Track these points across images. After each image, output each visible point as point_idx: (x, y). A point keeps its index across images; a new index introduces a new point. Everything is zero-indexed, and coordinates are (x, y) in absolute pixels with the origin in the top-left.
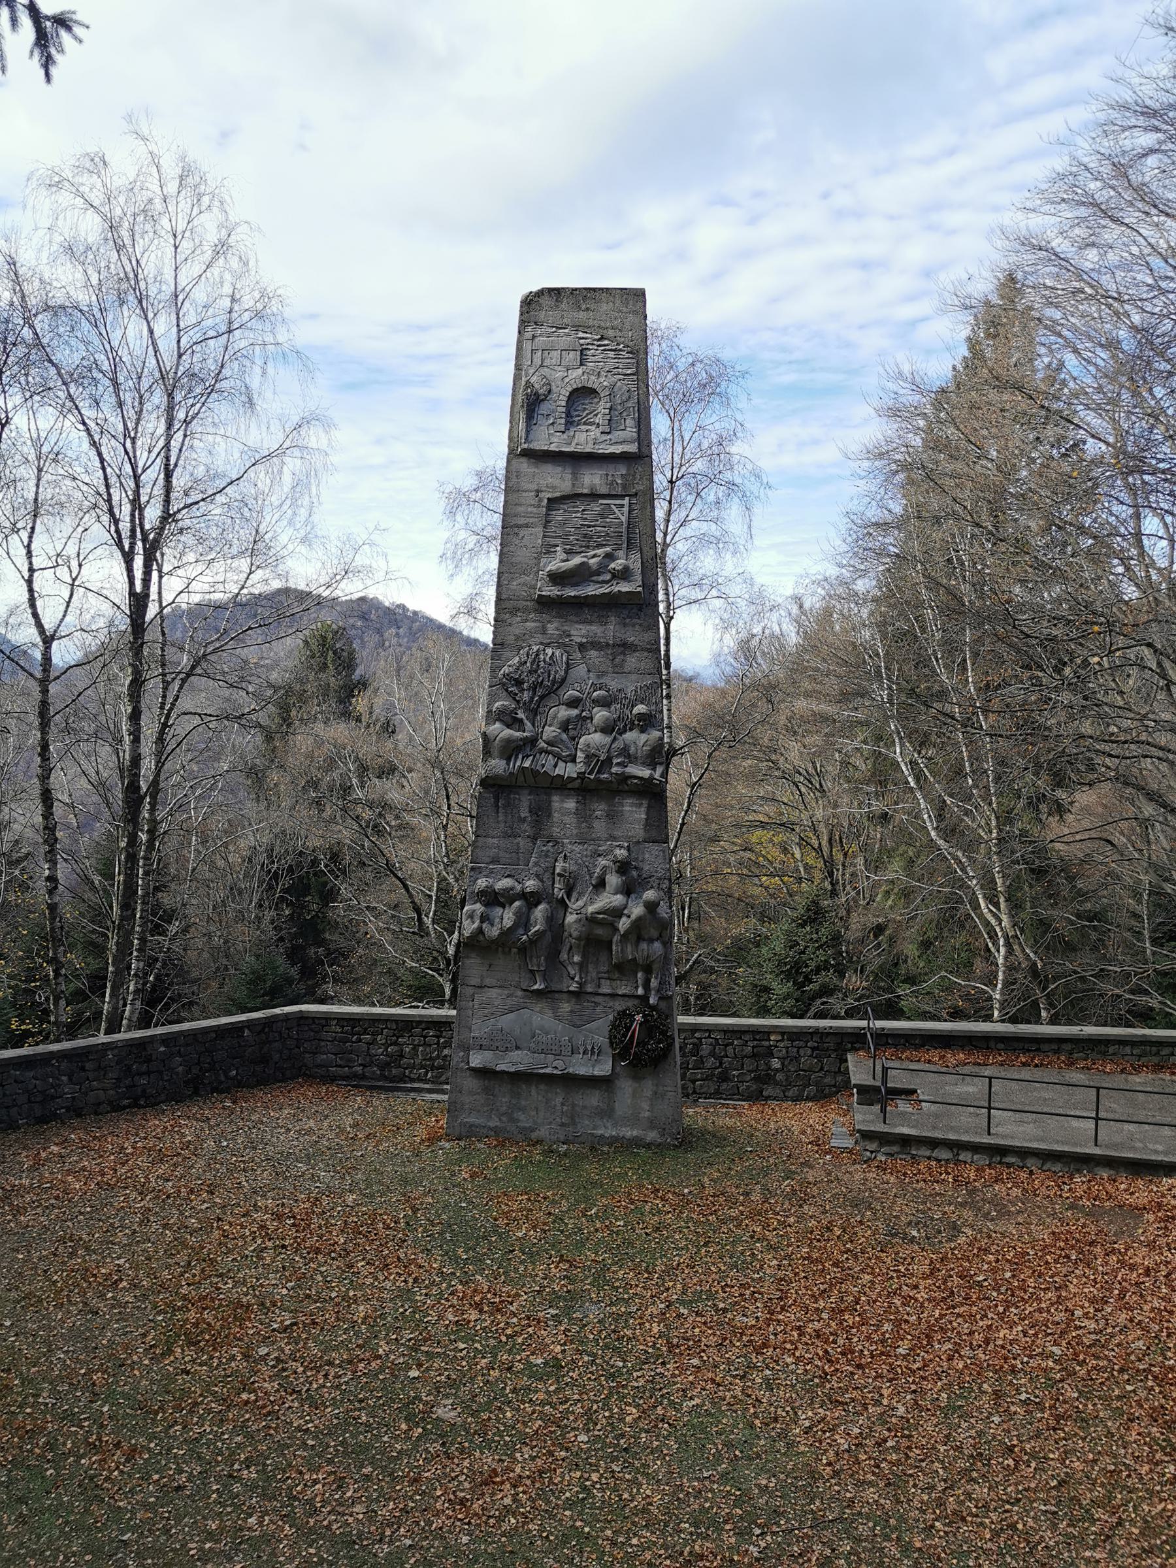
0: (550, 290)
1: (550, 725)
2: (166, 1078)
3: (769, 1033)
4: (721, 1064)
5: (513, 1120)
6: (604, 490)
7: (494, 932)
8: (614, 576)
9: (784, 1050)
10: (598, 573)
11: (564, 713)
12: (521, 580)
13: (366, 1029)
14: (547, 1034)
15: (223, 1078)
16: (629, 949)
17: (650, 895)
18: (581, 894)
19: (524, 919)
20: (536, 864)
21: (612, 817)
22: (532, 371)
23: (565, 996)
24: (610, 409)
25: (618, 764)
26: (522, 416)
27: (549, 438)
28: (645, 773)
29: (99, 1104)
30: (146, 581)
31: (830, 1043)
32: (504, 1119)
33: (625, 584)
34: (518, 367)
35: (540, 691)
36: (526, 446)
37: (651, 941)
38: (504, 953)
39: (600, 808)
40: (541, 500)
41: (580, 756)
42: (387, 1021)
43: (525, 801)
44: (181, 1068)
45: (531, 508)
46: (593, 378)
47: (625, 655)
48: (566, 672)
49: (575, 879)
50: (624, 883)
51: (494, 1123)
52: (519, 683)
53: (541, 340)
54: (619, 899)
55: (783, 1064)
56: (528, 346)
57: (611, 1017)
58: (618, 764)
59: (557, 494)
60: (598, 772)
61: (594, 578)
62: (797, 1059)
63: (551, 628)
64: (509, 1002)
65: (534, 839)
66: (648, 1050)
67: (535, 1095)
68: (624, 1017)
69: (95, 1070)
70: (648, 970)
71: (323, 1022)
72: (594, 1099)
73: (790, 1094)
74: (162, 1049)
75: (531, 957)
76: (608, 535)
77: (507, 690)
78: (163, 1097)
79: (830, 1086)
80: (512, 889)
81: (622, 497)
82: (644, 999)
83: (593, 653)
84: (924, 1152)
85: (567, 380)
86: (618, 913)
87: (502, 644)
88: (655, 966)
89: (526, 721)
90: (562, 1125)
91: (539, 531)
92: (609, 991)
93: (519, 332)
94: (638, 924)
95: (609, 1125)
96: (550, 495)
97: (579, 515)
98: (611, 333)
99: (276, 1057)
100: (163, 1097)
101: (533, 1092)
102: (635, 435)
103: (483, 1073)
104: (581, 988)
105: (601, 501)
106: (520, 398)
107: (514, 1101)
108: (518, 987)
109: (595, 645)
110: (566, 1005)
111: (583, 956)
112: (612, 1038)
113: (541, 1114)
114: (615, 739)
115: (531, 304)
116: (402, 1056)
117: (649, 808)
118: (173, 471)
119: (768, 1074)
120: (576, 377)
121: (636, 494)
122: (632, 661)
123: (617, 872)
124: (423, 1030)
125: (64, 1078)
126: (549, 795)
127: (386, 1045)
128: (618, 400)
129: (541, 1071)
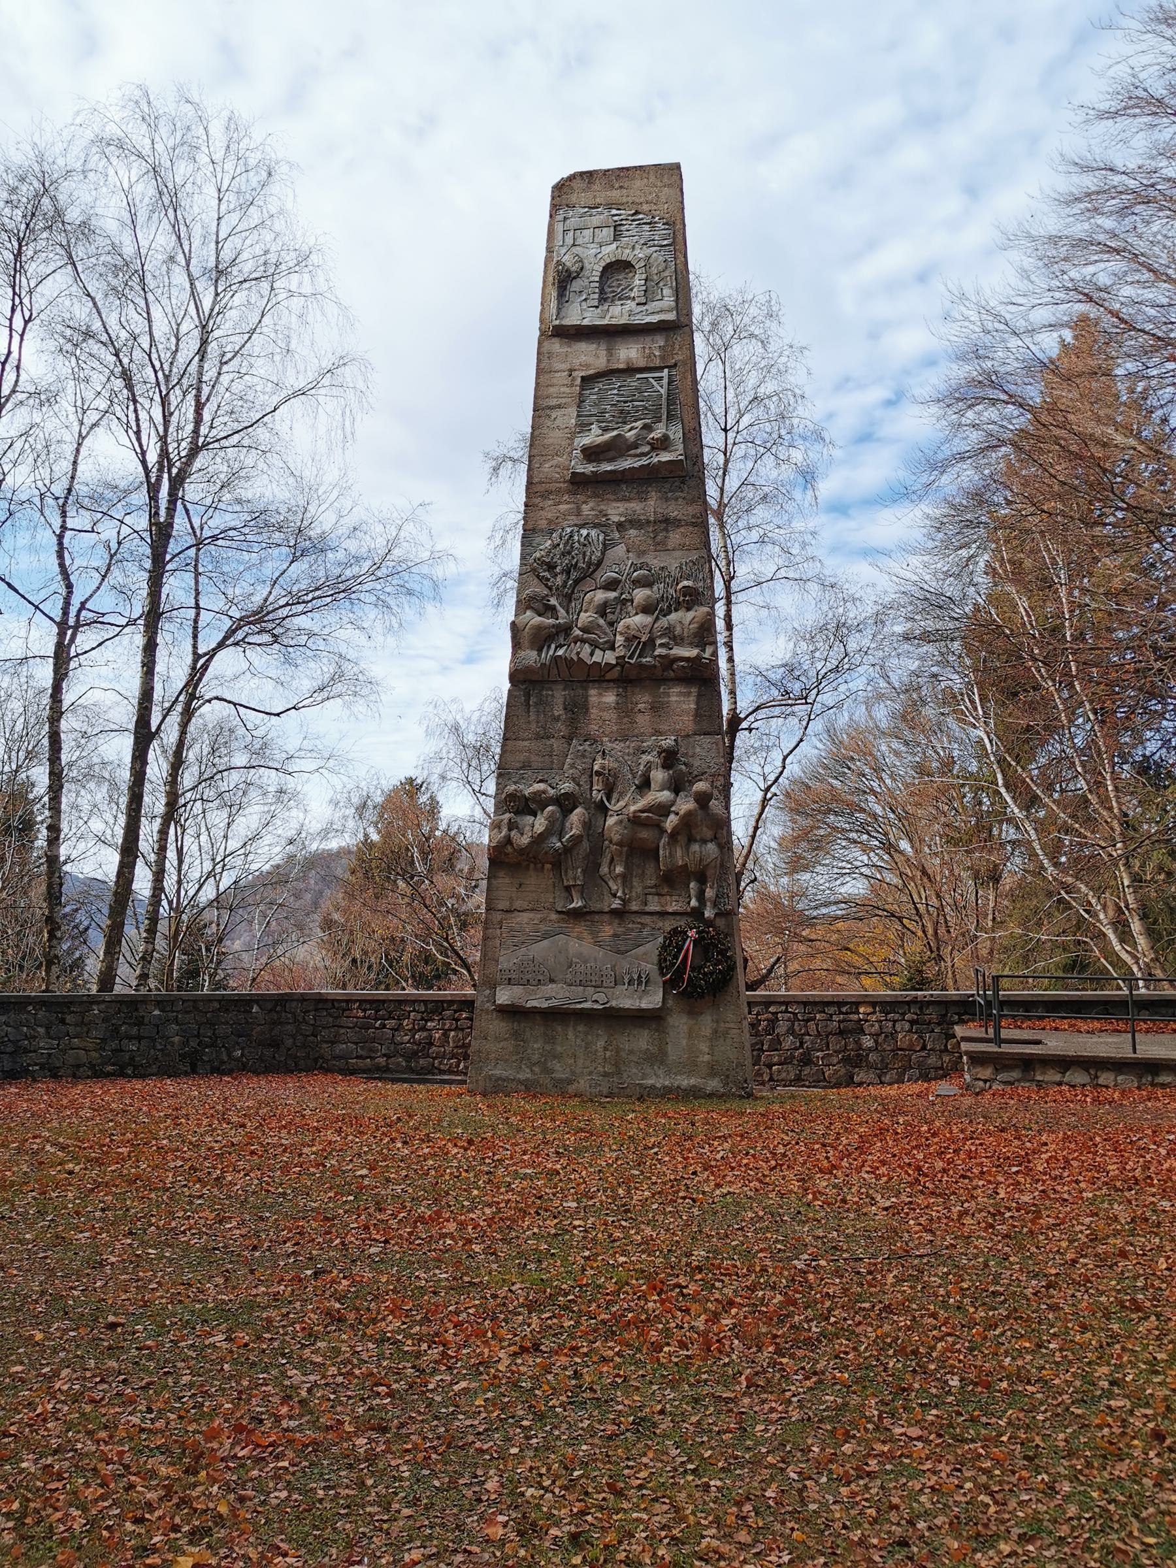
0: (582, 174)
1: (586, 611)
2: (159, 1047)
3: (857, 1004)
4: (802, 1043)
5: (547, 1071)
6: (642, 363)
7: (525, 840)
8: (654, 448)
9: (877, 1025)
10: (635, 446)
11: (601, 596)
12: (554, 462)
13: (391, 1013)
14: (585, 962)
15: (225, 1058)
16: (679, 853)
17: (700, 786)
18: (622, 795)
19: (557, 826)
20: (572, 766)
21: (657, 709)
22: (563, 251)
23: (606, 918)
24: (646, 280)
25: (662, 645)
26: (554, 294)
27: (580, 314)
28: (692, 653)
29: (78, 1066)
30: (171, 510)
31: (932, 1014)
32: (536, 1069)
33: (667, 454)
34: (549, 250)
35: (574, 575)
36: (557, 322)
37: (704, 841)
38: (535, 869)
39: (643, 700)
40: (574, 379)
41: (620, 639)
42: (414, 1001)
43: (559, 696)
44: (177, 1039)
45: (563, 388)
46: (627, 251)
47: (667, 531)
48: (603, 553)
49: (616, 777)
50: (671, 777)
51: (525, 1074)
52: (551, 567)
53: (573, 222)
54: (666, 795)
55: (876, 1042)
56: (559, 227)
57: (661, 940)
58: (662, 645)
59: (591, 372)
60: (640, 656)
61: (632, 452)
62: (893, 1035)
63: (586, 509)
64: (543, 927)
65: (569, 739)
66: (705, 974)
67: (571, 1037)
68: (675, 938)
69: (76, 1025)
70: (702, 879)
71: (344, 1005)
72: (642, 1040)
73: (887, 1078)
74: (157, 1012)
75: (566, 872)
76: (646, 408)
77: (538, 576)
78: (154, 1069)
79: (937, 1069)
80: (544, 792)
81: (661, 369)
82: (697, 913)
83: (633, 532)
84: (1053, 1076)
85: (600, 256)
86: (663, 810)
87: (534, 530)
88: (709, 873)
89: (559, 607)
90: (606, 1075)
91: (573, 411)
92: (658, 909)
93: (551, 216)
94: (687, 821)
95: (660, 1072)
96: (583, 374)
97: (615, 392)
98: (645, 207)
99: (289, 1042)
100: (154, 1069)
101: (571, 1036)
102: (673, 304)
103: (512, 1012)
104: (624, 905)
105: (638, 376)
106: (552, 274)
107: (548, 1047)
108: (552, 908)
109: (634, 523)
110: (607, 928)
111: (627, 867)
112: (661, 961)
113: (580, 1062)
114: (657, 619)
115: (563, 192)
116: (431, 1044)
117: (700, 696)
118: (204, 404)
119: (858, 1055)
120: (610, 252)
121: (675, 365)
122: (675, 537)
123: (663, 767)
124: (456, 1011)
125: (41, 1030)
126: (586, 689)
127: (413, 1031)
128: (654, 270)
129: (579, 1006)
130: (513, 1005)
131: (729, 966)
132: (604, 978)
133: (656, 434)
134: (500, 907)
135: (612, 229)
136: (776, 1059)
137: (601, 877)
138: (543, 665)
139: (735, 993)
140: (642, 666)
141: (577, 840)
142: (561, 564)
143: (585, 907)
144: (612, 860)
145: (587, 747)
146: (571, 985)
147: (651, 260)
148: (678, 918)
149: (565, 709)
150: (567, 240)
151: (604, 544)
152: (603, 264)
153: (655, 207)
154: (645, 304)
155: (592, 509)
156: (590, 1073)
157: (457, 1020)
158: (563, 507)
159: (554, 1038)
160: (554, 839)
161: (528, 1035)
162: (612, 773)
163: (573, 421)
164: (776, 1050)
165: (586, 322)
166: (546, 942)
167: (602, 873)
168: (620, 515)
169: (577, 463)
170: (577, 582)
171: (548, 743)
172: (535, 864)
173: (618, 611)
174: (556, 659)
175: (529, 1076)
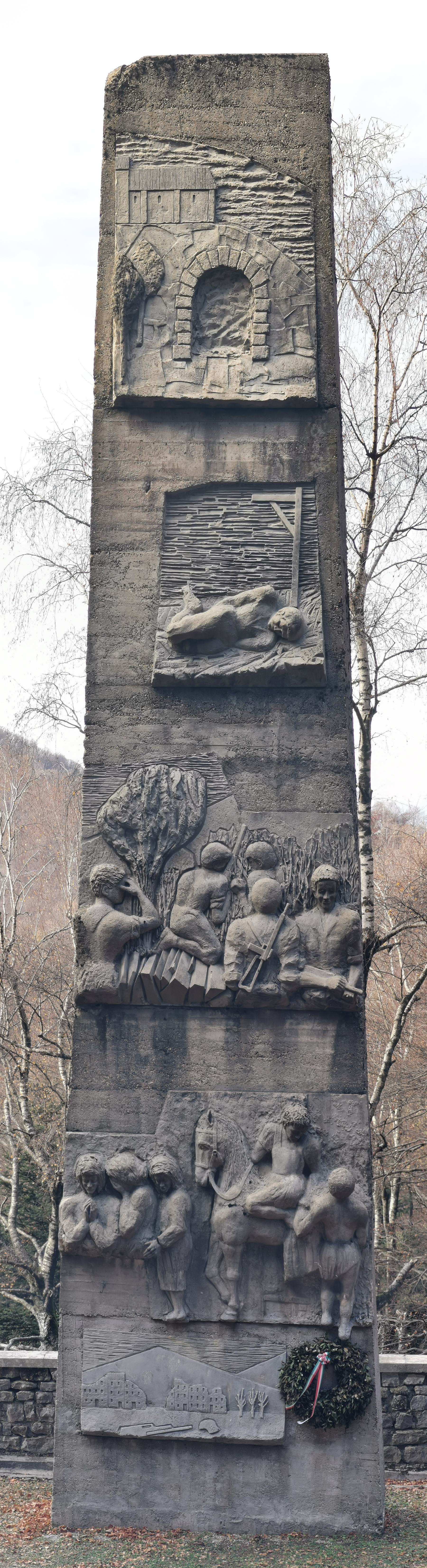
1: (182, 903)
5: (145, 1503)
6: (259, 474)
10: (251, 632)
14: (190, 1382)
18: (235, 1176)
19: (151, 1215)
20: (167, 1130)
22: (130, 236)
23: (215, 1328)
24: (269, 312)
25: (290, 966)
26: (117, 329)
34: (106, 229)
36: (124, 390)
37: (341, 1244)
40: (153, 498)
41: (230, 955)
48: (204, 811)
49: (226, 1152)
50: (300, 1157)
51: (120, 1507)
52: (129, 831)
54: (291, 1183)
57: (282, 1358)
58: (290, 966)
59: (181, 485)
60: (259, 980)
61: (247, 642)
63: (177, 732)
65: (162, 1090)
77: (110, 844)
80: (131, 1169)
83: (246, 777)
85: (192, 253)
86: (290, 1203)
90: (216, 1508)
91: (152, 555)
92: (280, 1319)
93: (106, 155)
94: (321, 1222)
96: (168, 487)
97: (218, 524)
102: (311, 362)
104: (238, 1316)
106: (112, 292)
107: (146, 1477)
109: (250, 762)
114: (284, 924)
117: (338, 1037)
124: (12, 1380)
126: (183, 1019)
130: (103, 1432)
132: (214, 1403)
133: (281, 617)
134: (79, 1311)
135: (211, 196)
136: (410, 1439)
137: (208, 1280)
138: (123, 986)
139: (372, 1421)
140: (259, 995)
141: (177, 1238)
142: (145, 827)
143: (188, 1316)
144: (222, 1257)
145: (186, 1105)
146: (174, 1409)
147: (277, 271)
148: (305, 1330)
149: (155, 1047)
150: (135, 212)
151: (206, 797)
152: (198, 272)
153: (283, 153)
154: (265, 360)
155: (187, 735)
156: (198, 1507)
157: (15, 1391)
158: (144, 729)
160: (147, 1233)
162: (222, 1147)
163: (154, 575)
164: (411, 1428)
165: (171, 393)
166: (138, 1358)
167: (209, 1275)
168: (229, 747)
169: (162, 655)
170: (167, 856)
171: (133, 1095)
173: (227, 903)
174: (141, 979)
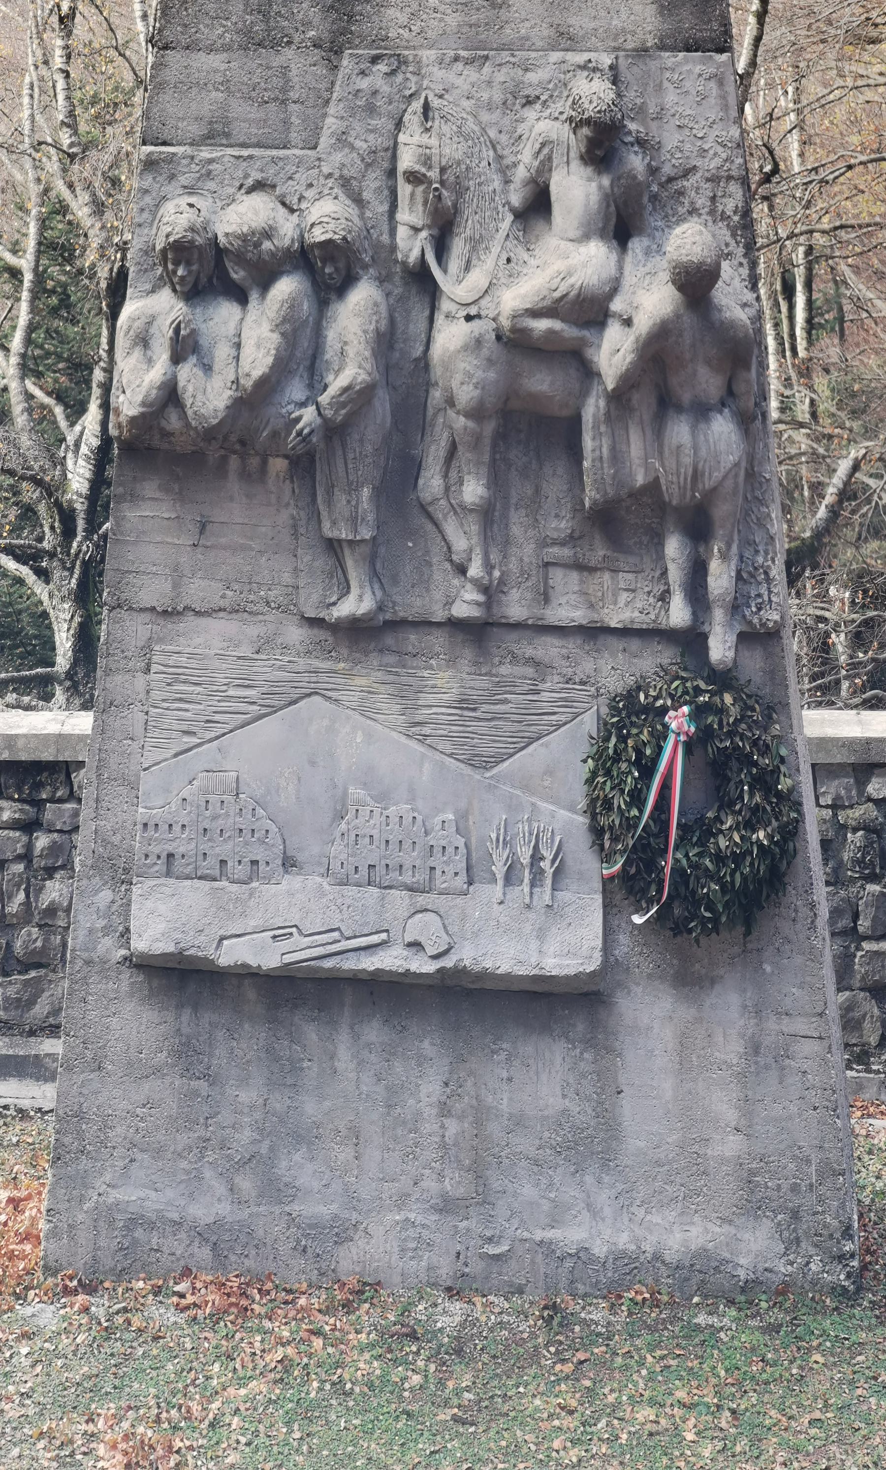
14: (383, 798)
18: (476, 244)
20: (342, 140)
23: (438, 641)
38: (245, 475)
49: (459, 189)
66: (719, 858)
75: (329, 503)
104: (488, 605)
107: (279, 1103)
130: (179, 956)
131: (782, 829)
139: (804, 911)
144: (452, 450)
156: (402, 1200)
159: (295, 1068)
161: (220, 1058)
171: (277, 61)
172: (243, 457)
175: (224, 1209)
